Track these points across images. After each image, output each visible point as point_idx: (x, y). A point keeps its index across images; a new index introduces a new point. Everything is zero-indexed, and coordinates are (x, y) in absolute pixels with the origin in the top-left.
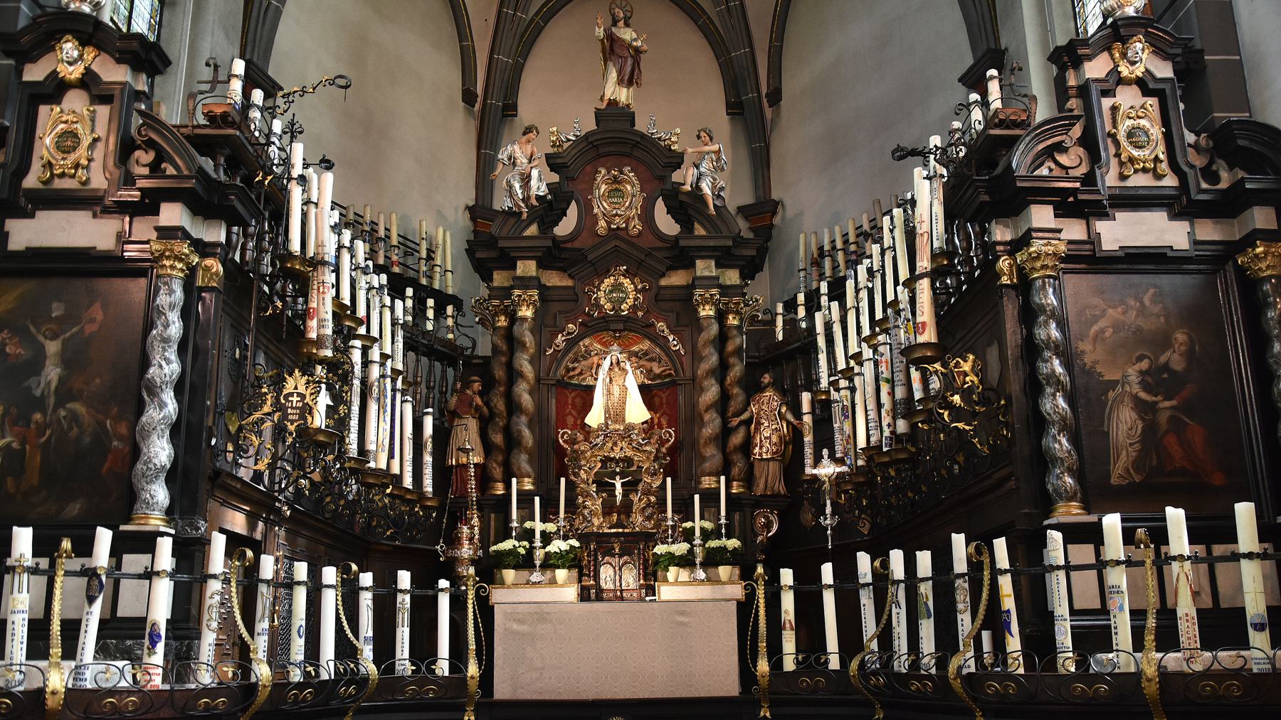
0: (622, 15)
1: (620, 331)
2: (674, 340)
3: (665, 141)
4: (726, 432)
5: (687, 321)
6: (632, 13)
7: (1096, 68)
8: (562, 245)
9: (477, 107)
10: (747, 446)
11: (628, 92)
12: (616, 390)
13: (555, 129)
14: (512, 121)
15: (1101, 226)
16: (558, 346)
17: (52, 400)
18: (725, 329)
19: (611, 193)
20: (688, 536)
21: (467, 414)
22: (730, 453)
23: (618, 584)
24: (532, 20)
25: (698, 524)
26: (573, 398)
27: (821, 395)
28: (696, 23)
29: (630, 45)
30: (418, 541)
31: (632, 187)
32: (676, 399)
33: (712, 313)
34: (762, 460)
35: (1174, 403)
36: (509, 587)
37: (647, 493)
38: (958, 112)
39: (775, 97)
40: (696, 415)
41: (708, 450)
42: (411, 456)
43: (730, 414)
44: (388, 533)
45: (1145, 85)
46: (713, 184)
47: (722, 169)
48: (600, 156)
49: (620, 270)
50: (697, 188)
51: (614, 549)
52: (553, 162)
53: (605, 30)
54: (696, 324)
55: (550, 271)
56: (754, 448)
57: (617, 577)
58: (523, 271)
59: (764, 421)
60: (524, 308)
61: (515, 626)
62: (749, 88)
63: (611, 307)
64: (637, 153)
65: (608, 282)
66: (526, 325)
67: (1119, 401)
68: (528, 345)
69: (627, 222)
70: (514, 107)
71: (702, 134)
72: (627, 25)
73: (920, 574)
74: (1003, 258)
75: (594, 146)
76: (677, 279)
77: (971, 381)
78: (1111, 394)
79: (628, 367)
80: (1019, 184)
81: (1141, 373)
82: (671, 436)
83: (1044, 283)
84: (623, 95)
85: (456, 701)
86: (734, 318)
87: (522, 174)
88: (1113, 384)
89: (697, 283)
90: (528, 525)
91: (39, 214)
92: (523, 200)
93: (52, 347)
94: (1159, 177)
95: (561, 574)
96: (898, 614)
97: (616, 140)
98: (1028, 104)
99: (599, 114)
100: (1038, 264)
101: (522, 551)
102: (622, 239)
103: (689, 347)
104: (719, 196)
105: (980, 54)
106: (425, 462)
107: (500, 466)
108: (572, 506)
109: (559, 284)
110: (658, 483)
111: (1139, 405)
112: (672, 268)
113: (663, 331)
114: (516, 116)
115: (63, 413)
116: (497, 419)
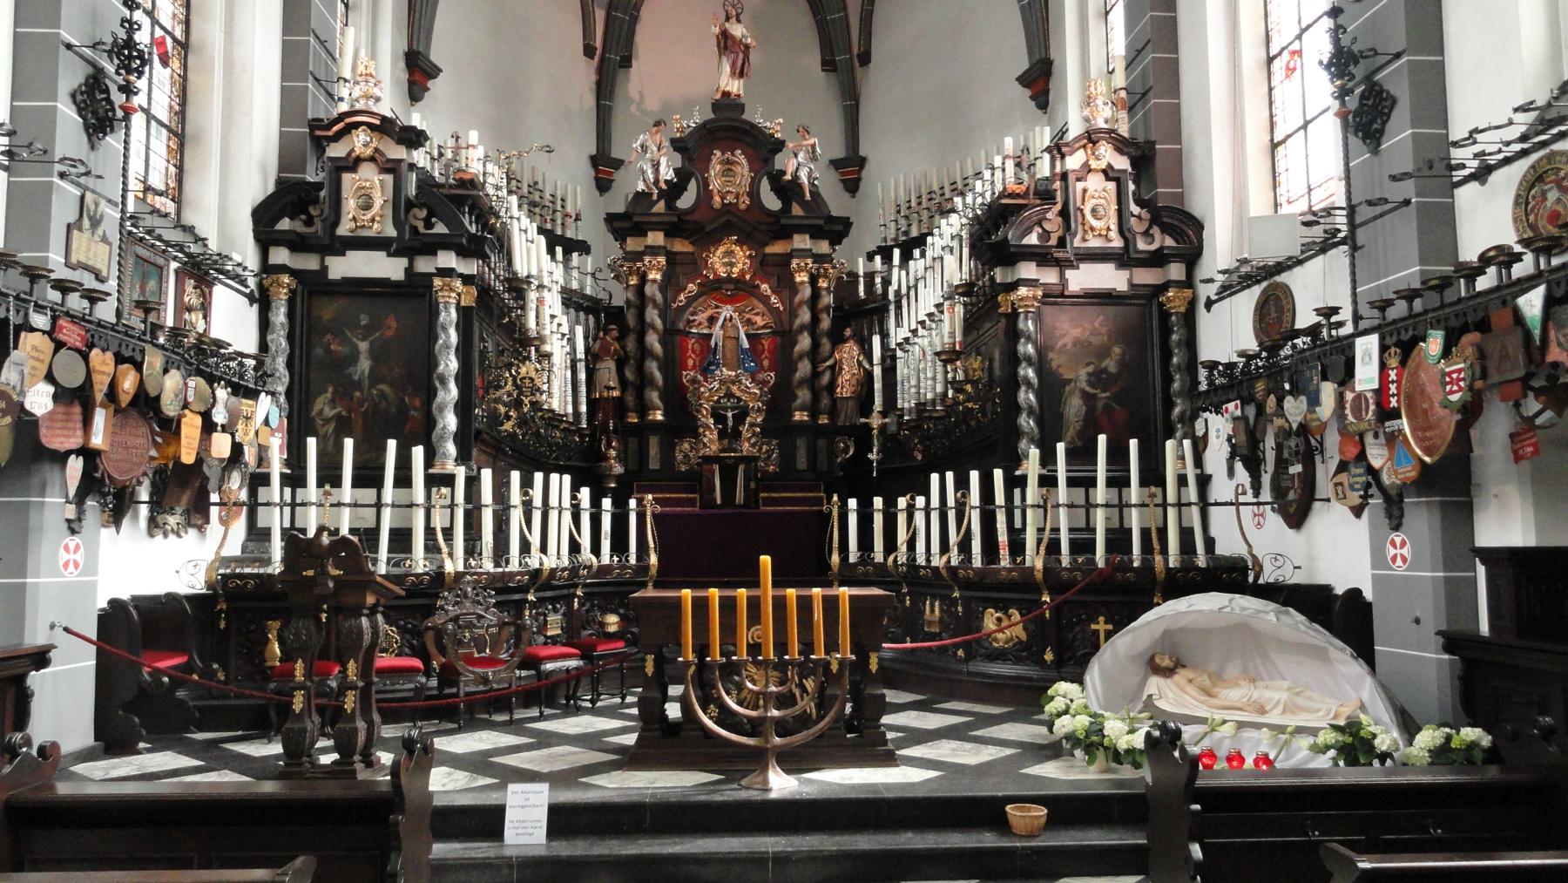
0: (734, 13)
4: (816, 374)
5: (785, 284)
7: (1074, 162)
9: (597, 58)
10: (832, 385)
13: (678, 117)
15: (1069, 274)
17: (367, 382)
26: (693, 344)
31: (743, 169)
33: (806, 279)
34: (843, 398)
35: (1107, 394)
39: (865, 58)
45: (1109, 173)
47: (817, 160)
50: (796, 177)
52: (678, 145)
54: (794, 288)
65: (722, 249)
67: (1072, 393)
69: (737, 197)
71: (801, 129)
72: (738, 21)
73: (932, 506)
76: (777, 248)
78: (1067, 388)
81: (1089, 374)
84: (735, 86)
88: (1070, 381)
89: (794, 253)
91: (348, 253)
93: (363, 346)
94: (1110, 241)
104: (813, 184)
105: (1035, 61)
111: (1085, 395)
114: (631, 66)
115: (375, 392)
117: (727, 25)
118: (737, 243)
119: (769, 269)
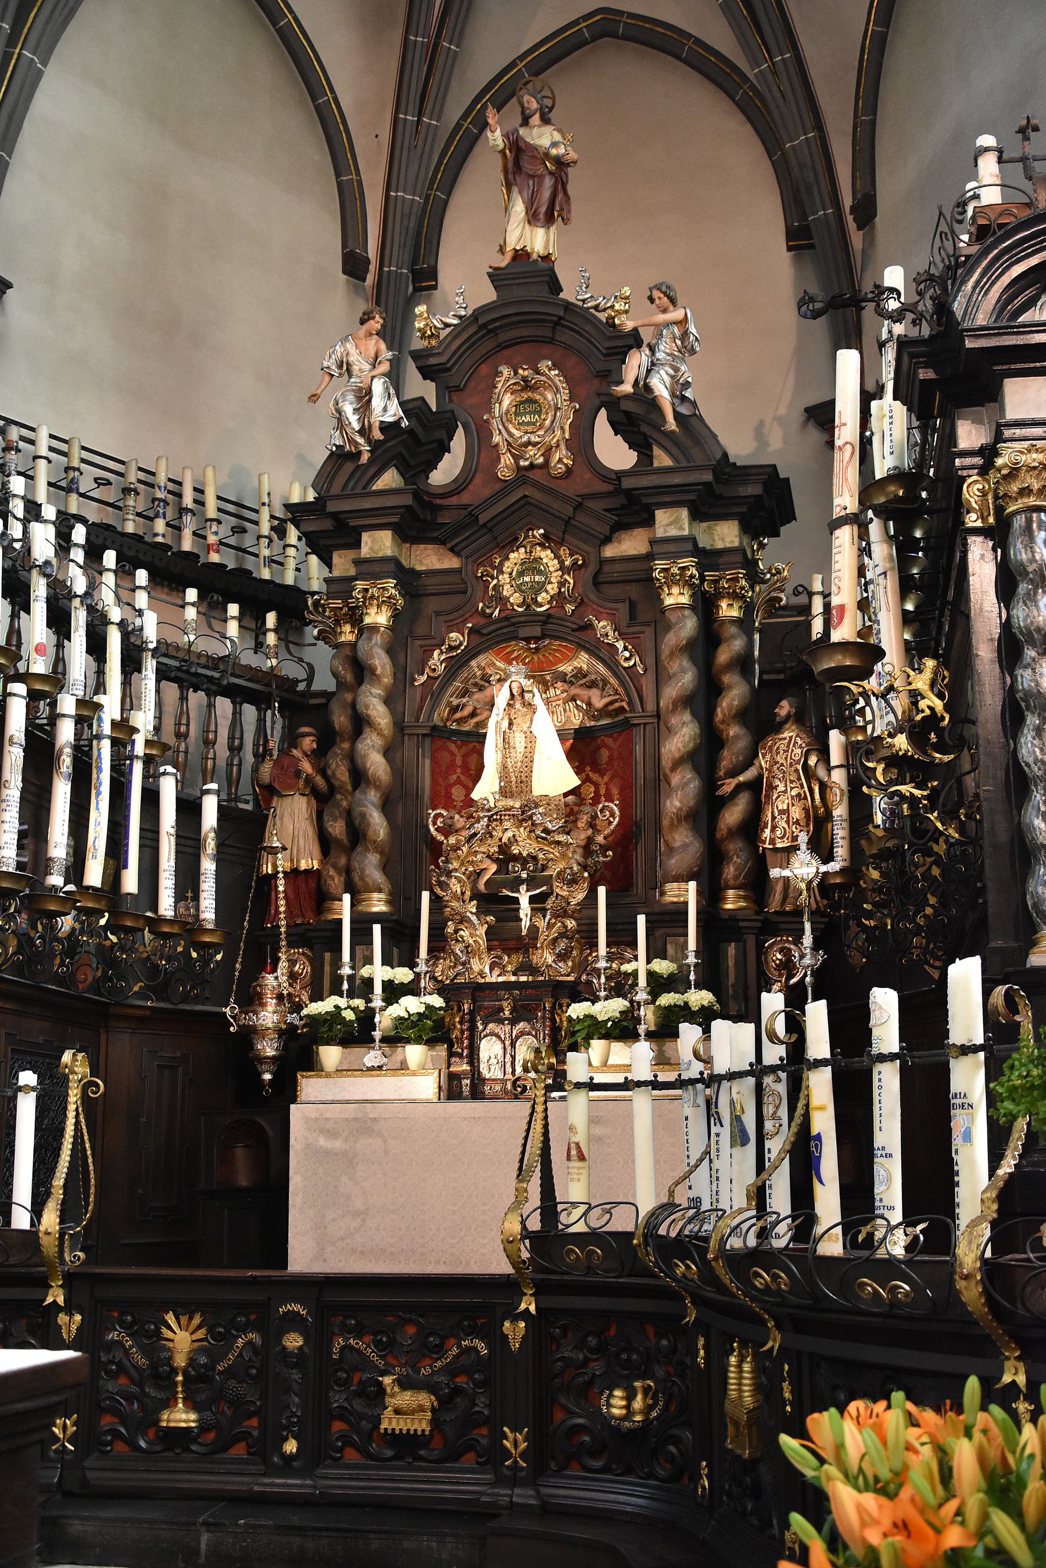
0: (535, 105)
1: (537, 639)
2: (625, 649)
3: (605, 310)
6: (553, 99)
8: (439, 502)
9: (370, 279)
11: (547, 234)
12: (519, 741)
14: (429, 297)
16: (434, 670)
18: (715, 626)
19: (519, 408)
20: (621, 985)
21: (290, 788)
22: (723, 840)
23: (509, 1070)
24: (458, 126)
25: (639, 966)
27: (856, 734)
28: (732, 99)
29: (547, 155)
30: (197, 1000)
32: (631, 752)
33: (684, 600)
34: (776, 850)
36: (328, 1075)
37: (562, 913)
38: (960, 217)
40: (661, 777)
41: (677, 837)
42: (173, 863)
43: (721, 773)
44: (136, 989)
46: (672, 377)
47: (692, 352)
48: (502, 347)
49: (534, 536)
51: (503, 1010)
53: (506, 136)
55: (422, 546)
56: (763, 831)
57: (508, 1059)
58: (371, 549)
59: (777, 782)
60: (373, 611)
61: (322, 1142)
62: (818, 202)
63: (521, 599)
64: (564, 336)
65: (516, 556)
66: (377, 639)
68: (378, 672)
69: (547, 453)
70: (432, 274)
71: (656, 294)
72: (546, 121)
74: (970, 480)
75: (490, 331)
77: (929, 707)
79: (538, 701)
80: (969, 344)
82: (612, 815)
83: (1029, 522)
85: (33, 1270)
86: (730, 605)
87: (360, 389)
90: (365, 972)
92: (362, 432)
95: (414, 1053)
96: (718, 1135)
97: (525, 317)
98: (1031, 192)
99: (496, 276)
100: (1015, 487)
101: (349, 1015)
102: (535, 484)
103: (650, 660)
104: (684, 399)
106: (202, 871)
107: (340, 874)
108: (439, 944)
109: (438, 566)
110: (581, 896)
112: (619, 527)
113: (607, 635)
116: (338, 797)
117: (522, 131)
118: (547, 541)
119: (616, 591)
